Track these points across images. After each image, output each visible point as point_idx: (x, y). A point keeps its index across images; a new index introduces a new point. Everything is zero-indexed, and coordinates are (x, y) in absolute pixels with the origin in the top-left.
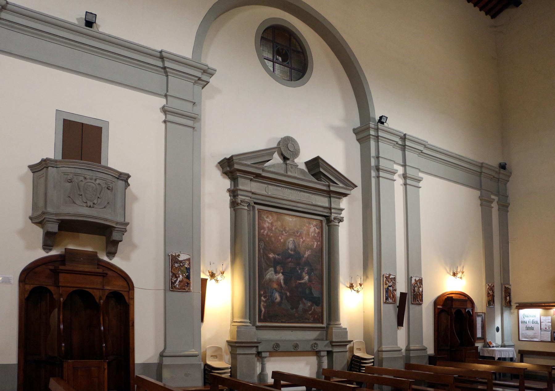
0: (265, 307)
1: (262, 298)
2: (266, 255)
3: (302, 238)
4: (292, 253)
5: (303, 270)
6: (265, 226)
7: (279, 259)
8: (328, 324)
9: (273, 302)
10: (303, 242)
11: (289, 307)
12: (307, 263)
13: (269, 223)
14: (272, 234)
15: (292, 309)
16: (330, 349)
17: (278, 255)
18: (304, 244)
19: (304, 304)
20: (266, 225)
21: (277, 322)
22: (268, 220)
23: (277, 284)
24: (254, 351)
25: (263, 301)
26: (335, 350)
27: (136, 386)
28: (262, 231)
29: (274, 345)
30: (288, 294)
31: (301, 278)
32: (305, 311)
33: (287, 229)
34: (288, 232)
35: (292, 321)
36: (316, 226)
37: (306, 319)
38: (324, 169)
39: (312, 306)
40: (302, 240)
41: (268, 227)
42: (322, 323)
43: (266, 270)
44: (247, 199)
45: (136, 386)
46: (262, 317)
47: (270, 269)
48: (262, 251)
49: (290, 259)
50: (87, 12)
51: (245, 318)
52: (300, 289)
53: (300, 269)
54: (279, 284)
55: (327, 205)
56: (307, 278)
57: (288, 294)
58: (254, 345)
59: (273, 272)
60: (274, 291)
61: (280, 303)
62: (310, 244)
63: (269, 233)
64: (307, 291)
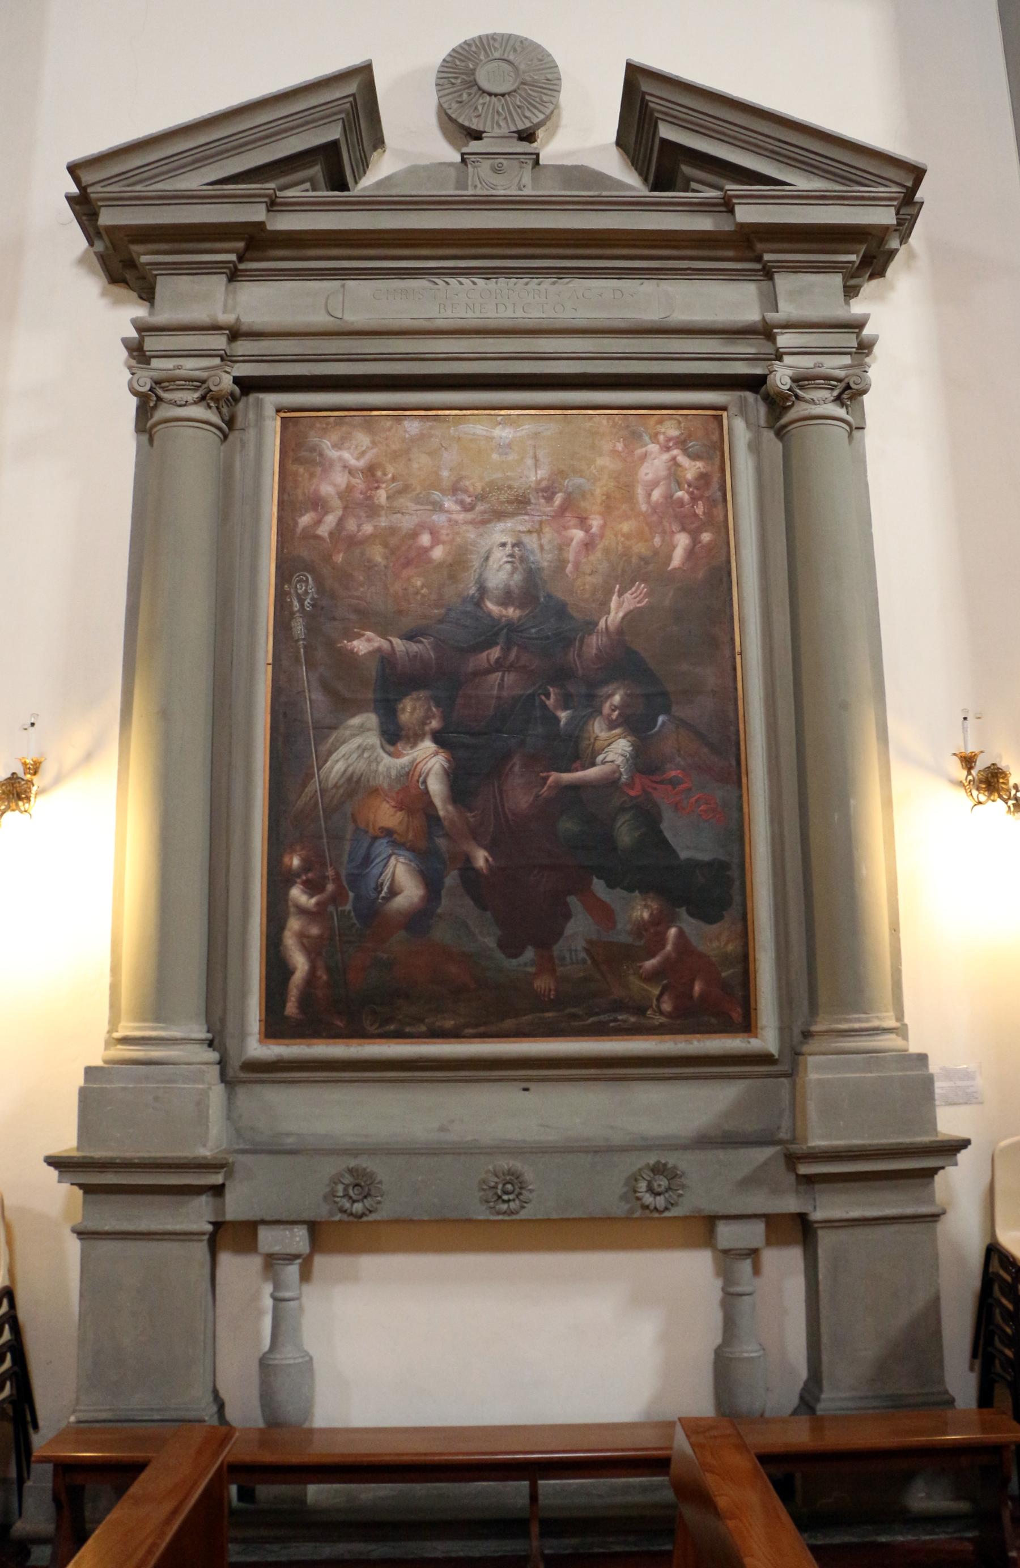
0: (312, 949)
1: (297, 894)
3: (583, 522)
4: (511, 612)
5: (589, 704)
6: (327, 489)
7: (414, 658)
8: (798, 1038)
9: (371, 912)
10: (588, 546)
12: (624, 661)
13: (351, 471)
15: (511, 947)
16: (790, 1204)
17: (411, 637)
18: (598, 554)
19: (605, 915)
20: (331, 486)
21: (399, 1035)
23: (400, 807)
24: (196, 1216)
25: (302, 911)
26: (826, 1208)
28: (305, 520)
29: (335, 1180)
30: (481, 858)
31: (576, 751)
32: (612, 957)
35: (509, 1024)
36: (681, 443)
37: (619, 1006)
38: (677, 123)
39: (661, 921)
40: (578, 535)
41: (347, 494)
42: (747, 1026)
43: (325, 729)
44: (190, 366)
46: (291, 1008)
47: (356, 721)
48: (299, 627)
49: (495, 653)
50: (918, 173)
51: (144, 1020)
52: (567, 825)
55: (752, 315)
56: (616, 751)
57: (481, 858)
58: (193, 1179)
59: (373, 739)
60: (382, 847)
61: (418, 920)
62: (639, 548)
63: (351, 525)
64: (625, 833)
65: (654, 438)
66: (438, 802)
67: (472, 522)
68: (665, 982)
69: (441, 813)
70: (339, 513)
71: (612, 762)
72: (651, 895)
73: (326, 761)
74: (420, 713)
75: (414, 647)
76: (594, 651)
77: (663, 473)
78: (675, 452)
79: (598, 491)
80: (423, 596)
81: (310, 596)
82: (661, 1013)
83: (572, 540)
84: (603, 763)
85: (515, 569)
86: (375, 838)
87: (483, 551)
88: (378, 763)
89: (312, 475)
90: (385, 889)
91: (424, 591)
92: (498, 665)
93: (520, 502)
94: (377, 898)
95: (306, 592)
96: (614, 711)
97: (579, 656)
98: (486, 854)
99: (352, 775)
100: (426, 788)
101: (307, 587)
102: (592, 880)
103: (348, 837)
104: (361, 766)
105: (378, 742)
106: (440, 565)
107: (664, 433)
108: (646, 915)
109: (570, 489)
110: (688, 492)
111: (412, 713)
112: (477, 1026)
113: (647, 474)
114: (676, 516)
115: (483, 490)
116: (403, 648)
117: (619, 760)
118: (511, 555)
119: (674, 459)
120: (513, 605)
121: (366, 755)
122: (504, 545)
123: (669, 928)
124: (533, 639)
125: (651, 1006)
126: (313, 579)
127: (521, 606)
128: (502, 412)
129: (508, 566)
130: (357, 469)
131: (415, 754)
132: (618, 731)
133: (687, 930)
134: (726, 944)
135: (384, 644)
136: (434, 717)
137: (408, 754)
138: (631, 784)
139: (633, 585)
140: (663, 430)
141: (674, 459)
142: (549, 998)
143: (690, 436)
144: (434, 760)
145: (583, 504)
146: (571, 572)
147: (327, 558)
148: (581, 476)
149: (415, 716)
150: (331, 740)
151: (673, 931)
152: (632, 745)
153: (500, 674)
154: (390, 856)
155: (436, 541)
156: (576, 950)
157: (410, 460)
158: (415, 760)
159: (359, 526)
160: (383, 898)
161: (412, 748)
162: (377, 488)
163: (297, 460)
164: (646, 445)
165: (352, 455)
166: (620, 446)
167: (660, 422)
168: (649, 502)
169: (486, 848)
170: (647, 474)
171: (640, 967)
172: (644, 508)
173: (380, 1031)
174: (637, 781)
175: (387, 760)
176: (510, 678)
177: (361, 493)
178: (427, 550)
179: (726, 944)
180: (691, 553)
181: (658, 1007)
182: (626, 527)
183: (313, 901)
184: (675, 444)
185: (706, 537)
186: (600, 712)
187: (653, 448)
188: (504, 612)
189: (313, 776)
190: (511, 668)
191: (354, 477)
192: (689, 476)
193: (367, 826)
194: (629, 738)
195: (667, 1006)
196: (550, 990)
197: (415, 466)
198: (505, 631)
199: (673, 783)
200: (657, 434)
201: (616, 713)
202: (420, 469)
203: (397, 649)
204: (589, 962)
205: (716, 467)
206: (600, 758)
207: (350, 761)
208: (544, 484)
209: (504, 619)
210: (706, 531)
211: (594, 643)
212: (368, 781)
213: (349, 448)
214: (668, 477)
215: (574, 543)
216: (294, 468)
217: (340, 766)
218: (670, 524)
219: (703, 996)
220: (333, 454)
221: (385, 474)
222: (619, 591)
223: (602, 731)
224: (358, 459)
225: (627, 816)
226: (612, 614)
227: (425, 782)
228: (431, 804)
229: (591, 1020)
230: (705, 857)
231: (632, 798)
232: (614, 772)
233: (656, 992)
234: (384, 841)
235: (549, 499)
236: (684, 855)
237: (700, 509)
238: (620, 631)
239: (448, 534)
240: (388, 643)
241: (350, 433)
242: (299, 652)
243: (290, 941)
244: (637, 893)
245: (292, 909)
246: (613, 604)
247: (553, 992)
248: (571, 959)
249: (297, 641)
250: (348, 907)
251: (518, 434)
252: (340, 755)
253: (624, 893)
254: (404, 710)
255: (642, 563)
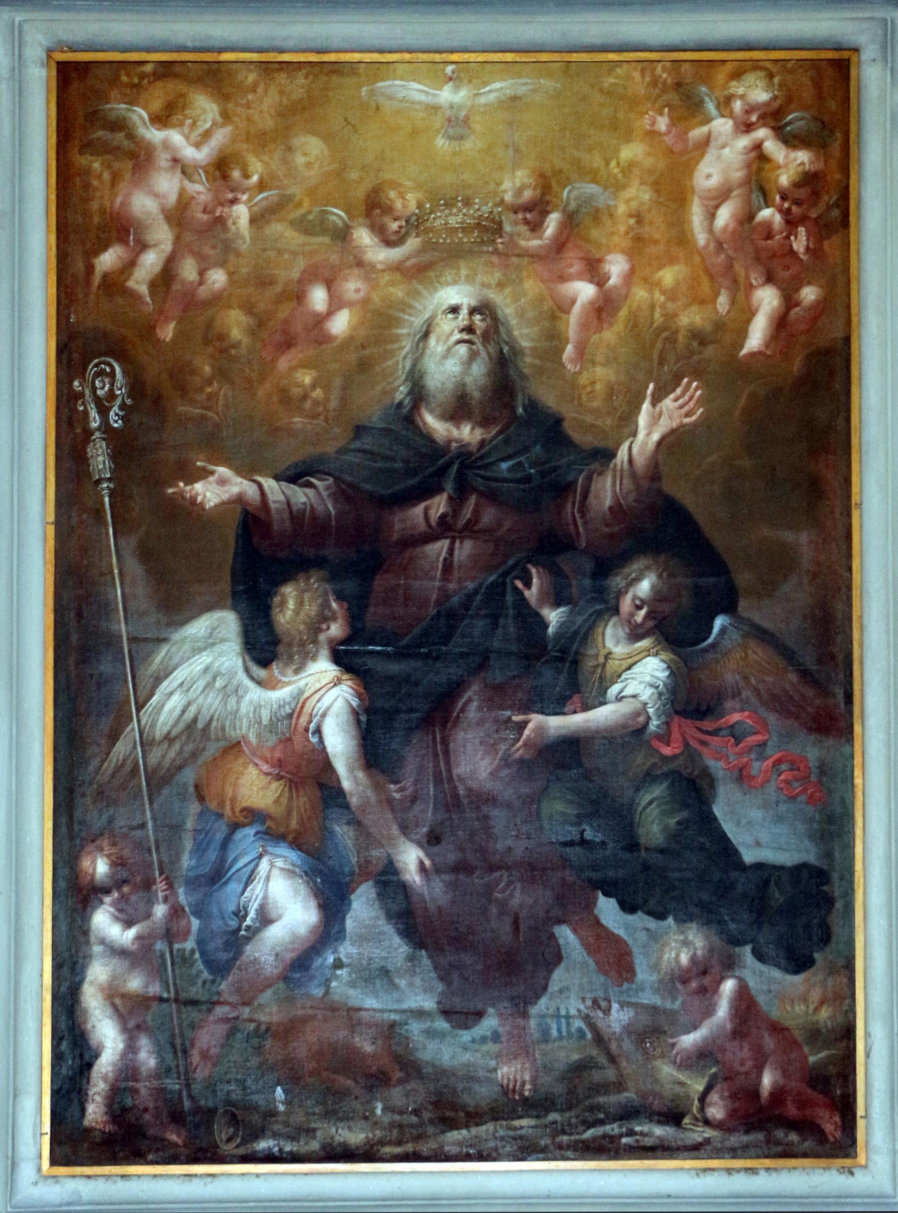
0: (130, 1011)
3: (593, 270)
4: (467, 433)
7: (296, 516)
10: (603, 309)
12: (659, 524)
14: (218, 278)
17: (296, 476)
19: (616, 961)
20: (149, 201)
27: (651, 386)
28: (108, 259)
33: (407, 202)
34: (415, 224)
36: (773, 117)
40: (584, 291)
41: (178, 215)
45: (651, 386)
46: (95, 1112)
47: (199, 627)
48: (100, 458)
49: (439, 505)
50: (73, 1144)
54: (308, 772)
56: (640, 678)
59: (229, 656)
62: (691, 318)
63: (188, 270)
64: (655, 820)
65: (725, 104)
66: (341, 767)
67: (397, 268)
68: (714, 1070)
69: (346, 784)
70: (167, 247)
71: (634, 696)
72: (694, 925)
73: (152, 695)
74: (311, 609)
75: (300, 496)
76: (608, 502)
77: (738, 175)
78: (762, 133)
79: (622, 209)
80: (316, 403)
81: (118, 402)
82: (707, 1122)
83: (574, 302)
84: (619, 699)
85: (473, 356)
86: (235, 827)
87: (418, 322)
88: (240, 699)
89: (116, 178)
90: (252, 914)
91: (318, 393)
92: (445, 527)
93: (485, 229)
94: (239, 929)
95: (111, 396)
96: (639, 608)
97: (583, 514)
98: (421, 854)
99: (195, 720)
100: (321, 740)
101: (112, 385)
102: (596, 899)
103: (189, 825)
104: (211, 704)
105: (240, 662)
106: (348, 341)
107: (742, 97)
108: (684, 959)
109: (573, 206)
110: (780, 211)
111: (297, 612)
112: (399, 1143)
113: (709, 176)
114: (757, 259)
115: (420, 206)
116: (282, 498)
117: (647, 694)
118: (469, 329)
119: (758, 147)
120: (470, 418)
121: (219, 684)
122: (455, 310)
123: (721, 980)
124: (505, 480)
125: (689, 1112)
126: (125, 372)
127: (485, 422)
128: (455, 57)
129: (463, 349)
130: (196, 167)
131: (302, 683)
132: (645, 643)
133: (752, 983)
134: (816, 1010)
135: (249, 489)
136: (334, 619)
137: (289, 683)
138: (665, 737)
139: (678, 384)
140: (741, 91)
141: (758, 147)
142: (521, 1094)
143: (789, 100)
144: (336, 691)
145: (594, 234)
146: (572, 361)
147: (148, 331)
148: (594, 181)
149: (302, 616)
150: (158, 659)
151: (729, 986)
152: (669, 667)
153: (445, 543)
154: (260, 856)
155: (336, 304)
156: (568, 1017)
157: (290, 149)
158: (301, 692)
159: (202, 273)
160: (248, 928)
161: (297, 671)
162: (233, 202)
163: (88, 147)
164: (708, 120)
165: (187, 138)
166: (662, 123)
167: (737, 75)
168: (710, 230)
169: (419, 844)
170: (709, 176)
171: (673, 1045)
172: (701, 238)
173: (241, 1151)
174: (676, 734)
175: (254, 694)
176: (465, 550)
177: (204, 212)
178: (320, 320)
179: (816, 1010)
180: (781, 323)
181: (702, 1109)
182: (668, 276)
183: (132, 932)
184: (762, 117)
185: (809, 294)
186: (616, 611)
187: (722, 126)
188: (455, 433)
189: (131, 720)
190: (470, 530)
191: (191, 181)
192: (784, 180)
193: (222, 803)
194: (664, 655)
195: (716, 1112)
196: (524, 1083)
197: (300, 160)
198: (455, 467)
199: (736, 735)
200: (728, 100)
201: (643, 612)
202: (308, 165)
203: (271, 497)
204: (589, 1036)
205: (833, 164)
206: (614, 690)
207: (192, 695)
208: (528, 194)
209: (454, 445)
210: (809, 283)
211: (606, 491)
212: (223, 729)
213: (181, 125)
214: (747, 182)
215: (577, 309)
216: (83, 160)
217: (175, 703)
218: (747, 269)
219: (778, 1095)
220: (155, 135)
221: (247, 176)
222: (653, 395)
223: (617, 643)
224: (198, 145)
225: (658, 791)
226: (641, 436)
227: (318, 731)
228: (327, 766)
229: (589, 1134)
230: (786, 858)
231: (664, 759)
232: (637, 714)
233: (699, 1086)
234: (250, 831)
235: (536, 227)
236: (749, 856)
237: (800, 243)
238: (654, 472)
239: (357, 291)
240: (255, 487)
241: (182, 95)
242: (103, 504)
243: (92, 1000)
244: (670, 920)
245: (97, 949)
246: (643, 420)
247: (528, 1087)
248: (559, 1030)
249: (98, 482)
250: (190, 944)
251: (483, 100)
252: (175, 684)
253: (651, 923)
254: (283, 603)
255: (695, 344)
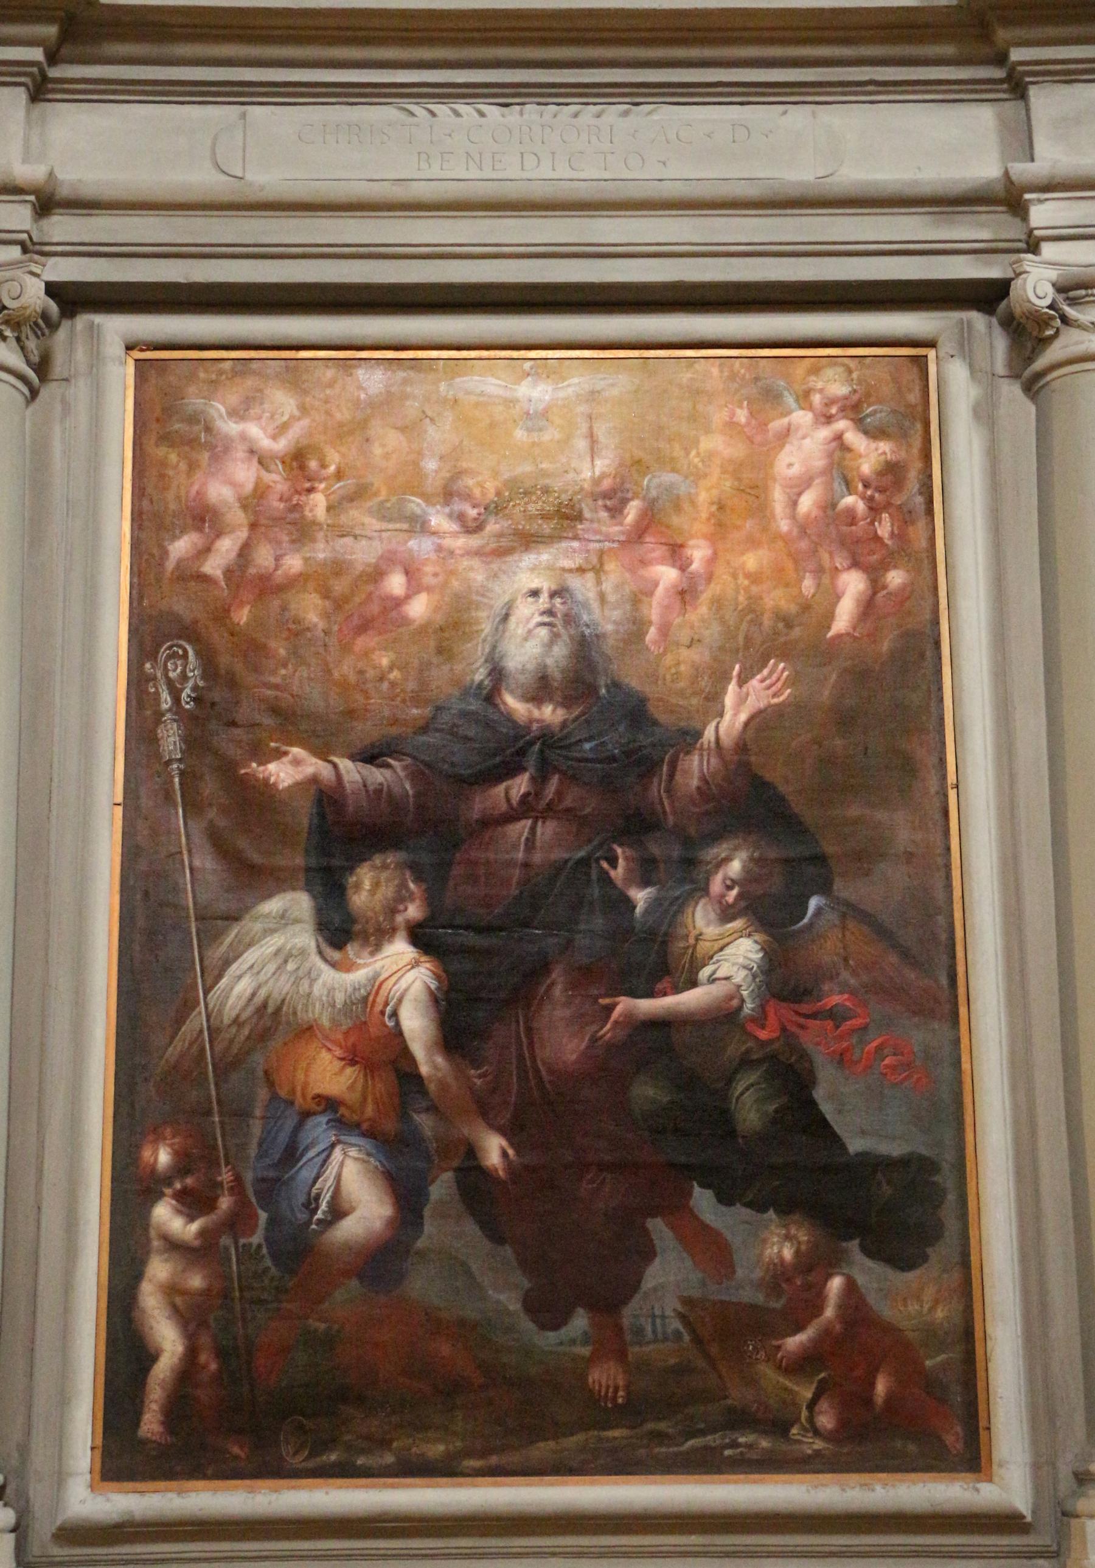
0: (191, 1315)
1: (166, 1215)
2: (228, 770)
3: (676, 553)
4: (550, 714)
5: (688, 875)
6: (219, 492)
9: (298, 1248)
10: (685, 594)
11: (505, 1295)
12: (749, 800)
13: (263, 460)
15: (547, 1310)
17: (371, 756)
19: (714, 1252)
22: (253, 428)
25: (174, 1246)
27: (737, 667)
28: (181, 547)
30: (494, 1149)
31: (661, 960)
32: (729, 1330)
35: (543, 1450)
37: (739, 1419)
39: (814, 1265)
41: (253, 501)
42: (973, 1459)
43: (216, 921)
45: (737, 667)
46: (151, 1424)
47: (273, 905)
49: (520, 785)
52: (647, 1092)
53: (646, 871)
57: (494, 1149)
59: (304, 938)
60: (319, 1130)
61: (382, 1261)
62: (775, 599)
64: (751, 1106)
